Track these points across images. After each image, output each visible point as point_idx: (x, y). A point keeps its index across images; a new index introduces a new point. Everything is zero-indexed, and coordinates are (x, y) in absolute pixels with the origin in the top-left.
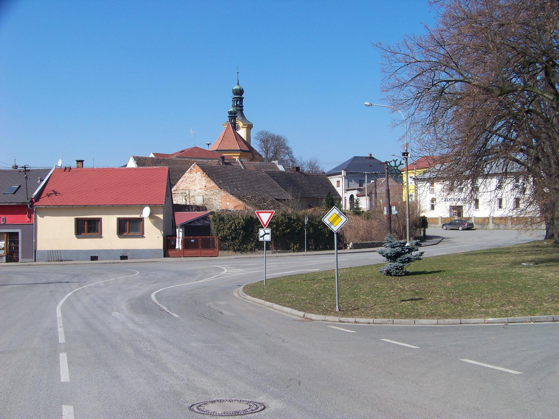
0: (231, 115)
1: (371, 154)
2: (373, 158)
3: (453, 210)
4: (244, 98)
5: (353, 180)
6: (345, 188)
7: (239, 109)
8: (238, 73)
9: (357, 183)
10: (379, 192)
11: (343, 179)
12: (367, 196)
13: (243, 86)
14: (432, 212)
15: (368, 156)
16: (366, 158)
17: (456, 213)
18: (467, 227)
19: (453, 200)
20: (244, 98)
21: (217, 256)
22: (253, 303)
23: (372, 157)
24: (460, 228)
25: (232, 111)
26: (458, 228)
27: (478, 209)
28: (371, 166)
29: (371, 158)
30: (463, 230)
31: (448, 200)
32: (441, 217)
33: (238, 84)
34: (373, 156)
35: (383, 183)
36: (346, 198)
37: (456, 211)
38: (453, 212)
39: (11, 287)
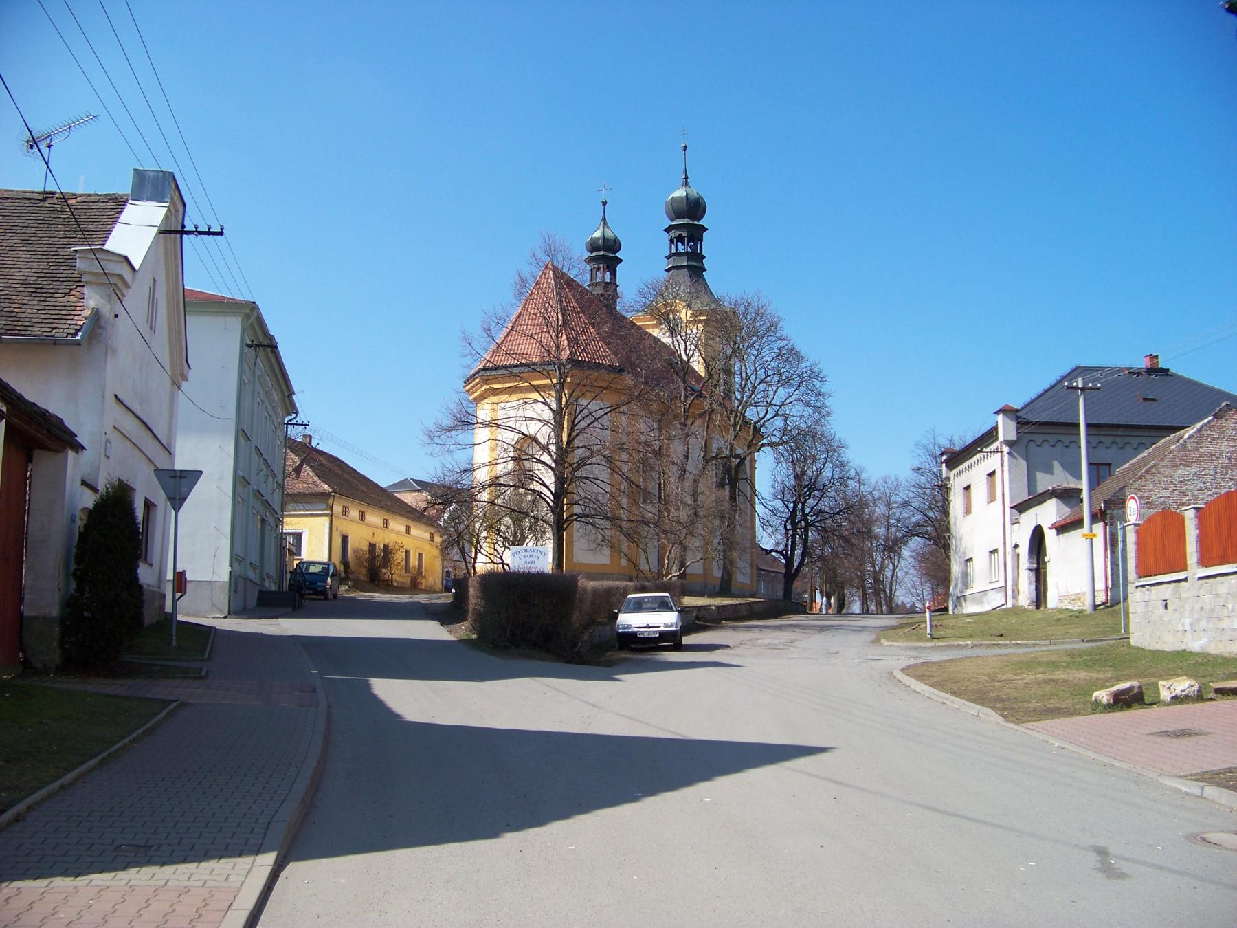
0: (594, 254)
1: (1154, 357)
2: (1165, 372)
4: (620, 261)
5: (1056, 464)
6: (1011, 502)
8: (685, 148)
9: (1012, 421)
10: (1165, 493)
11: (1006, 457)
12: (1095, 518)
15: (1143, 364)
16: (1133, 372)
22: (1037, 642)
23: (1161, 368)
25: (598, 239)
28: (1153, 400)
29: (1155, 371)
33: (686, 183)
34: (1162, 364)
35: (1189, 447)
36: (543, 554)
39: (905, 622)
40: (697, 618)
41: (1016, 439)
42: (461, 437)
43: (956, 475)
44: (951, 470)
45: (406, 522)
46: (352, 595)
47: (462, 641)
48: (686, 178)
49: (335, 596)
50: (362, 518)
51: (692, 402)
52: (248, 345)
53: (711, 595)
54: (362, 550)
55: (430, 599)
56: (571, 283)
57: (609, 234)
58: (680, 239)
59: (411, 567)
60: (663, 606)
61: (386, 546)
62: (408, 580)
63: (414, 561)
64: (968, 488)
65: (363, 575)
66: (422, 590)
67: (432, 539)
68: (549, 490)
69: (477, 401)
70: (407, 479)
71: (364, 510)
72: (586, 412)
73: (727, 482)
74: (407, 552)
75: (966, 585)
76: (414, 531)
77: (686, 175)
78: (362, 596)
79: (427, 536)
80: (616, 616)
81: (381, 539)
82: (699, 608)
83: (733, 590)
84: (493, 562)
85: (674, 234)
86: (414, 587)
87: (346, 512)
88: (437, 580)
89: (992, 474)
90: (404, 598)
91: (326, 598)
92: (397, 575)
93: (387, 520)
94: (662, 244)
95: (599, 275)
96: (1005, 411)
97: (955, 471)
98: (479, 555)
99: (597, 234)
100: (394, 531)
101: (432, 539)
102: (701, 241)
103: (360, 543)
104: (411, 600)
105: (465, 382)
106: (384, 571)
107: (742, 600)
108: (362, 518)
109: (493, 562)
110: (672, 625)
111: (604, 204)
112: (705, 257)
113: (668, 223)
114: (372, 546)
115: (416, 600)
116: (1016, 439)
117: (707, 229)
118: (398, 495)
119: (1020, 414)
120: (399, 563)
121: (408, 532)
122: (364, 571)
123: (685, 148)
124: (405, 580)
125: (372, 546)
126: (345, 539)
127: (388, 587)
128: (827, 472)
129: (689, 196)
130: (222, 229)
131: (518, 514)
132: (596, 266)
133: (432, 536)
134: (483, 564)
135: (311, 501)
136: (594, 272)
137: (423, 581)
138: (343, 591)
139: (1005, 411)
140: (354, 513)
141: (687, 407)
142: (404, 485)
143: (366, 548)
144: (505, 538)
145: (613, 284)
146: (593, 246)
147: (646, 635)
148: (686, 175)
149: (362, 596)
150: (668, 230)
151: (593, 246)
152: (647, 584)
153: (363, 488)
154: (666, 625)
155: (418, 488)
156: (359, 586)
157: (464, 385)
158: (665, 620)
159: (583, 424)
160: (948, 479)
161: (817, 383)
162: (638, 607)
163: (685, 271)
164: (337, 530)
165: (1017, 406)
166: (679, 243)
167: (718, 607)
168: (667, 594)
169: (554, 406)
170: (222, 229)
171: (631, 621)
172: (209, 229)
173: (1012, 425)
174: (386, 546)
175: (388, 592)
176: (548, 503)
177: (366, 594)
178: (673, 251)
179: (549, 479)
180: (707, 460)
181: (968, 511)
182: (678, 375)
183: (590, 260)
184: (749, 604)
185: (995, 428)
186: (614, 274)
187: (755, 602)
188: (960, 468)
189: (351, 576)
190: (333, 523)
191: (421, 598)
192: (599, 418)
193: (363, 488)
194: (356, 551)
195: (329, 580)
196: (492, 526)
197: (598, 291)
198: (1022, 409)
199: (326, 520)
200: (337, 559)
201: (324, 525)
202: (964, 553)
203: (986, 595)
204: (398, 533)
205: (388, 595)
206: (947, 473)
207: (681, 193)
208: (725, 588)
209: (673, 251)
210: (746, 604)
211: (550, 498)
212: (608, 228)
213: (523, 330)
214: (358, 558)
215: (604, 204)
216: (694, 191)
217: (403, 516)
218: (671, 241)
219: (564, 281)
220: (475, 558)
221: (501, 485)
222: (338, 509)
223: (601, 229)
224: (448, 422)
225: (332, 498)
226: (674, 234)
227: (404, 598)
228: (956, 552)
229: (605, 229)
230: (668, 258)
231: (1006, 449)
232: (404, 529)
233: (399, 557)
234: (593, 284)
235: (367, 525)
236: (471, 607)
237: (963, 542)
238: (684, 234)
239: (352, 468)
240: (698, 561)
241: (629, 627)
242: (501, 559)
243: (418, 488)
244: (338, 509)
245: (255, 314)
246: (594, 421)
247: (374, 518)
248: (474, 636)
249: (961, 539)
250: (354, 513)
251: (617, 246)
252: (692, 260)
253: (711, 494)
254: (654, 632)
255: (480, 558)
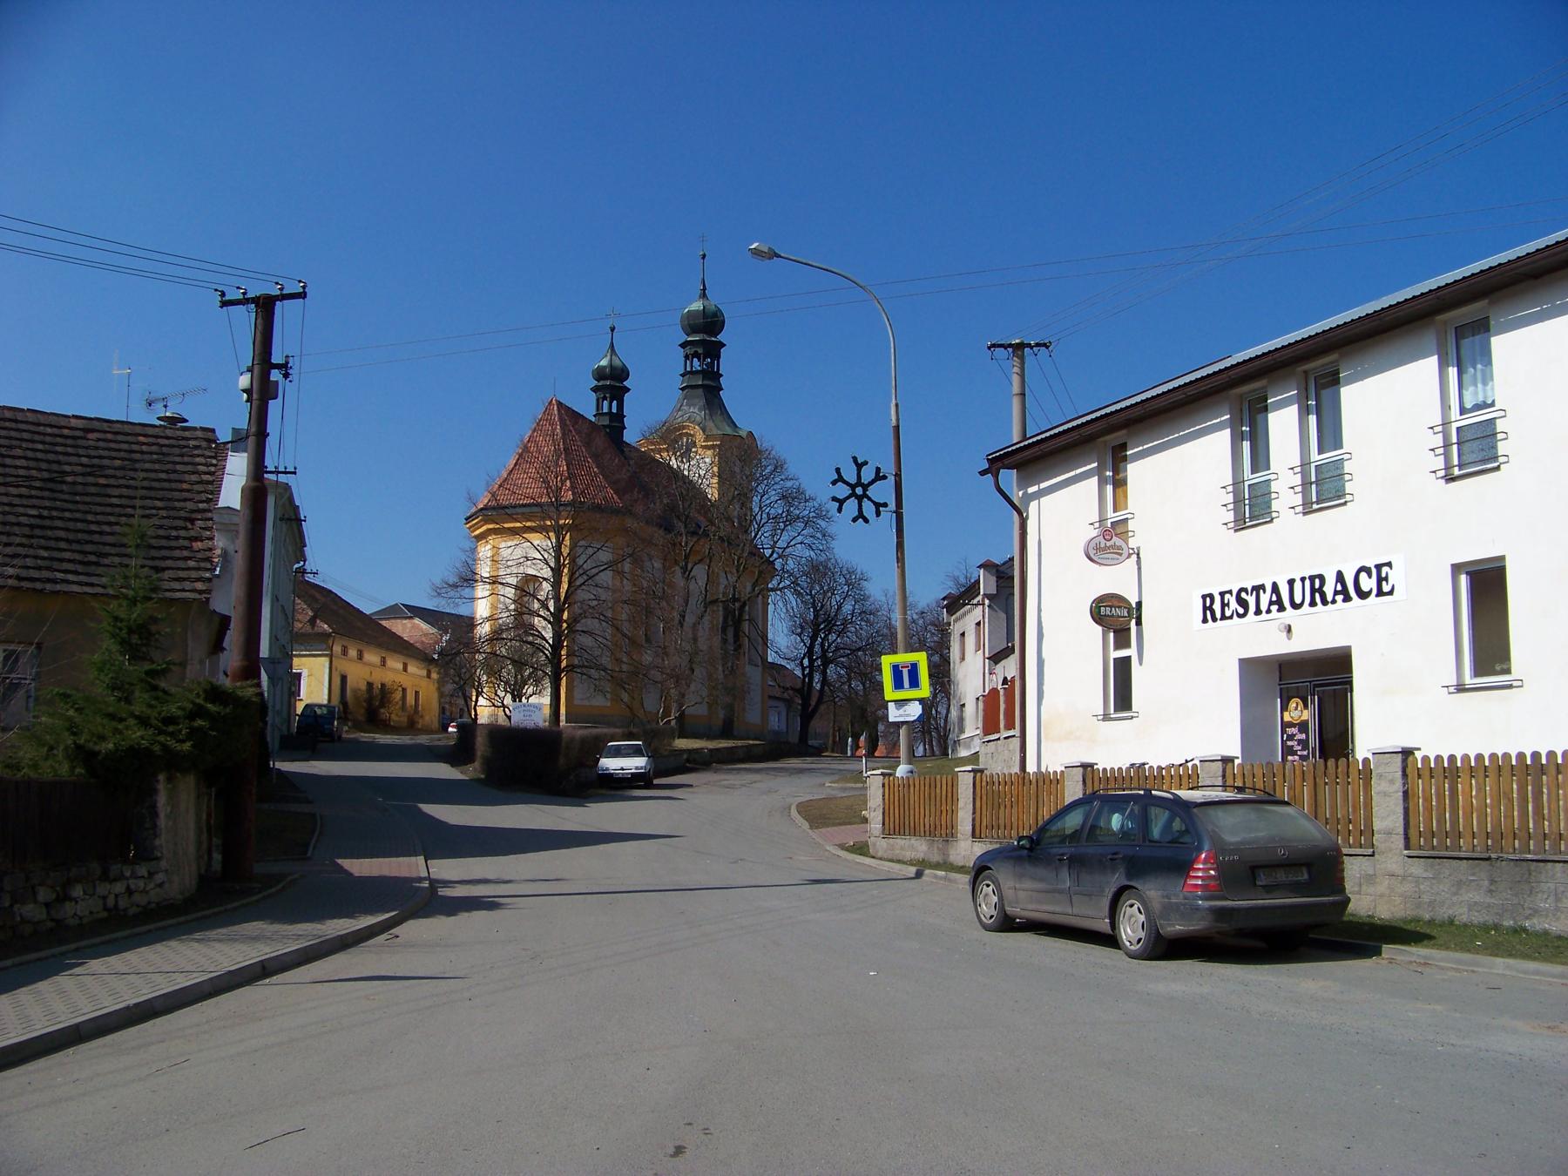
3: (1284, 708)
4: (628, 390)
7: (700, 383)
8: (704, 257)
13: (626, 358)
14: (1119, 728)
17: (1303, 726)
18: (1220, 913)
19: (1265, 599)
20: (628, 390)
21: (1407, 847)
24: (1131, 929)
25: (604, 367)
26: (1103, 925)
27: (1508, 671)
30: (1165, 948)
31: (1224, 605)
32: (1407, 753)
33: (704, 295)
37: (1306, 715)
38: (1285, 725)
40: (688, 761)
41: (995, 592)
42: (466, 592)
43: (955, 621)
44: (952, 615)
45: (402, 659)
46: (352, 736)
47: (471, 780)
48: (704, 289)
49: (340, 737)
50: (360, 657)
51: (692, 548)
52: (281, 519)
53: (710, 737)
54: (360, 690)
55: (432, 740)
56: (576, 416)
57: (617, 362)
58: (696, 355)
59: (408, 704)
60: (637, 752)
61: (383, 685)
62: (405, 719)
63: (410, 699)
64: (963, 634)
65: (360, 714)
66: (419, 730)
67: (429, 676)
68: (547, 642)
69: (480, 538)
70: (397, 604)
71: (360, 648)
72: (581, 571)
73: (731, 623)
74: (404, 690)
75: (962, 730)
76: (411, 669)
77: (704, 286)
78: (365, 737)
79: (424, 673)
80: (598, 760)
81: (379, 677)
82: (690, 751)
83: (735, 733)
84: (494, 705)
85: (689, 350)
86: (411, 726)
87: (345, 652)
88: (433, 718)
89: (978, 624)
90: (406, 740)
91: (333, 741)
92: (396, 716)
93: (384, 658)
94: (676, 361)
95: (606, 403)
96: (986, 566)
97: (954, 617)
98: (480, 698)
99: (604, 363)
100: (391, 669)
101: (429, 676)
102: (719, 357)
103: (358, 683)
104: (413, 741)
105: (466, 519)
106: (382, 710)
107: (740, 743)
108: (360, 657)
109: (494, 705)
110: (641, 768)
111: (613, 329)
112: (721, 375)
113: (684, 338)
114: (370, 685)
115: (418, 741)
116: (995, 592)
117: (725, 345)
118: (384, 623)
119: (1001, 569)
120: (397, 703)
121: (405, 669)
122: (363, 711)
123: (704, 257)
124: (402, 719)
125: (370, 685)
126: (344, 678)
127: (386, 727)
128: (847, 608)
129: (706, 310)
130: (295, 468)
131: (519, 664)
132: (602, 395)
133: (429, 673)
134: (485, 711)
135: (315, 641)
136: (601, 400)
137: (420, 721)
138: (348, 734)
139: (986, 566)
140: (353, 653)
141: (688, 551)
142: (394, 611)
143: (363, 687)
144: (506, 683)
145: (618, 418)
146: (600, 374)
147: (620, 776)
148: (704, 286)
149: (365, 737)
150: (683, 345)
151: (600, 374)
152: (635, 730)
153: (359, 624)
154: (637, 768)
155: (409, 614)
156: (358, 727)
157: (465, 521)
158: (635, 764)
159: (578, 583)
160: (949, 624)
161: (823, 524)
162: (618, 753)
163: (700, 391)
164: (336, 670)
165: (998, 561)
166: (695, 360)
167: (711, 750)
168: (640, 743)
169: (552, 565)
170: (295, 468)
171: (611, 764)
172: (286, 468)
173: (993, 580)
174: (383, 685)
175: (386, 733)
176: (546, 655)
177: (367, 735)
178: (688, 369)
179: (548, 634)
180: (709, 603)
181: (963, 659)
182: (679, 519)
183: (595, 390)
184: (746, 746)
185: (978, 582)
186: (621, 406)
187: (753, 745)
188: (958, 614)
189: (350, 717)
190: (333, 663)
191: (423, 739)
192: (593, 576)
193: (359, 624)
194: (355, 691)
195: (336, 723)
196: (494, 673)
197: (606, 421)
198: (1004, 564)
199: (325, 661)
200: (336, 701)
201: (324, 666)
202: (960, 699)
203: (972, 740)
204: (394, 670)
205: (389, 736)
206: (947, 618)
207: (697, 306)
208: (726, 731)
209: (688, 369)
210: (742, 746)
211: (548, 651)
212: (616, 355)
213: (529, 494)
214: (356, 697)
215: (613, 329)
216: (715, 300)
217: (400, 653)
218: (687, 357)
219: (569, 416)
220: (477, 701)
221: (504, 639)
222: (337, 649)
223: (609, 357)
224: (453, 579)
225: (332, 639)
226: (689, 350)
227: (406, 740)
228: (954, 697)
229: (613, 357)
230: (683, 375)
231: (987, 602)
232: (400, 666)
233: (398, 695)
234: (598, 414)
235: (365, 664)
236: (479, 753)
237: (960, 686)
238: (700, 351)
239: (345, 601)
240: (693, 706)
241: (607, 769)
242: (502, 702)
243: (409, 614)
244: (337, 649)
245: (288, 494)
246: (588, 580)
247: (372, 657)
248: (483, 776)
249: (958, 684)
250: (353, 653)
251: (624, 375)
252: (710, 379)
253: (708, 638)
254: (627, 774)
255: (482, 701)
